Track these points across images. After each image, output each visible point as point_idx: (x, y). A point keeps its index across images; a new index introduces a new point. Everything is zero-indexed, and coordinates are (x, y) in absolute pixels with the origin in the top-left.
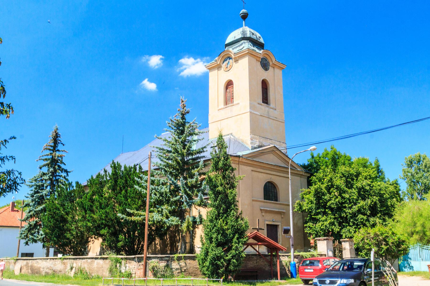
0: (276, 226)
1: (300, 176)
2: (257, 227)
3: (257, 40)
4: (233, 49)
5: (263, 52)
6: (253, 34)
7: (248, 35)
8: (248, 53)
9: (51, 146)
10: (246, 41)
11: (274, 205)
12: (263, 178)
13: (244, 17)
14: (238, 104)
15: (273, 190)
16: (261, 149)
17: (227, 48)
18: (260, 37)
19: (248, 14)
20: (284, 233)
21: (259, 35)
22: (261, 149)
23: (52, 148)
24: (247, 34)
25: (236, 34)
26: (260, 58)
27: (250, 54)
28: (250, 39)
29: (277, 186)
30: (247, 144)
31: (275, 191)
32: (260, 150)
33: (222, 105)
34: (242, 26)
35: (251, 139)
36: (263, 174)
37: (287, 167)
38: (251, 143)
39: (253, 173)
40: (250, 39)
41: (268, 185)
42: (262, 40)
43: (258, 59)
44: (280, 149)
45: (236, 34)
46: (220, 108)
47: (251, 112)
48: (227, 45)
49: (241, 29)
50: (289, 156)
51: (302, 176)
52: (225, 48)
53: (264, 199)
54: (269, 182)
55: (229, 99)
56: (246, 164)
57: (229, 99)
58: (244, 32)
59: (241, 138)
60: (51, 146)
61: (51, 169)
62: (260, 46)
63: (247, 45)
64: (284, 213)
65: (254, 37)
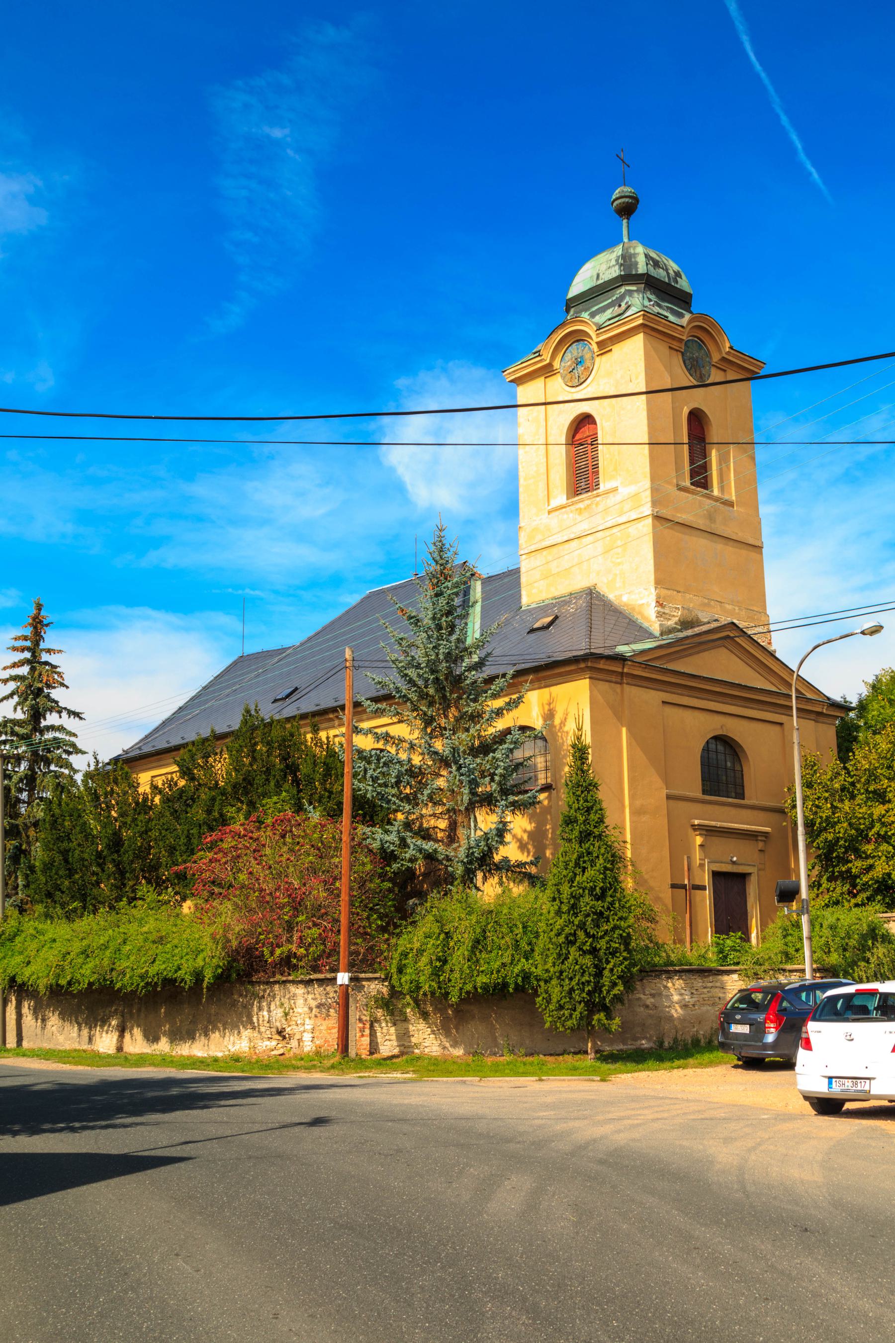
0: (742, 878)
1: (813, 716)
2: (686, 882)
3: (669, 284)
4: (593, 315)
5: (690, 322)
6: (656, 264)
7: (642, 268)
8: (643, 325)
9: (25, 638)
10: (634, 288)
11: (733, 811)
12: (696, 726)
13: (627, 210)
14: (615, 490)
15: (729, 764)
16: (689, 632)
17: (572, 311)
18: (678, 274)
19: (636, 200)
20: (779, 902)
21: (675, 267)
22: (689, 632)
23: (27, 655)
24: (636, 263)
25: (600, 268)
26: (681, 340)
27: (651, 328)
28: (650, 283)
29: (743, 751)
30: (647, 619)
31: (738, 768)
32: (687, 638)
33: (560, 498)
34: (620, 240)
35: (659, 604)
36: (697, 713)
37: (784, 691)
38: (660, 615)
39: (669, 710)
40: (650, 283)
41: (712, 746)
42: (684, 284)
43: (675, 345)
44: (749, 632)
45: (600, 268)
46: (554, 503)
47: (657, 518)
48: (570, 304)
49: (618, 250)
50: (777, 655)
51: (821, 719)
52: (568, 311)
53: (704, 792)
54: (716, 738)
55: (583, 478)
56: (645, 684)
57: (583, 478)
58: (627, 260)
59: (625, 599)
60: (25, 638)
61: (32, 832)
62: (682, 300)
63: (638, 302)
64: (765, 835)
65: (660, 274)
